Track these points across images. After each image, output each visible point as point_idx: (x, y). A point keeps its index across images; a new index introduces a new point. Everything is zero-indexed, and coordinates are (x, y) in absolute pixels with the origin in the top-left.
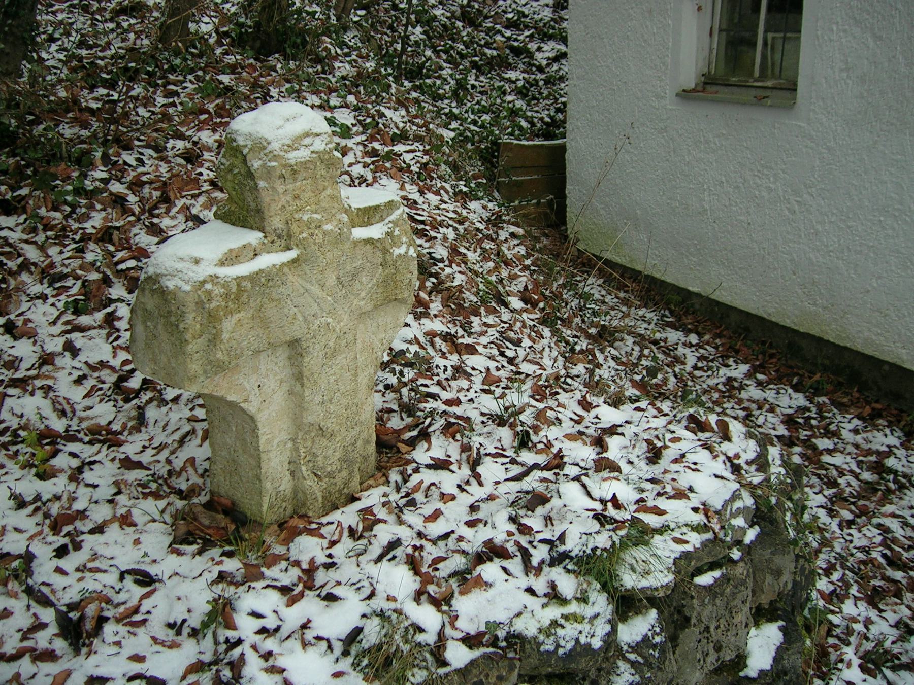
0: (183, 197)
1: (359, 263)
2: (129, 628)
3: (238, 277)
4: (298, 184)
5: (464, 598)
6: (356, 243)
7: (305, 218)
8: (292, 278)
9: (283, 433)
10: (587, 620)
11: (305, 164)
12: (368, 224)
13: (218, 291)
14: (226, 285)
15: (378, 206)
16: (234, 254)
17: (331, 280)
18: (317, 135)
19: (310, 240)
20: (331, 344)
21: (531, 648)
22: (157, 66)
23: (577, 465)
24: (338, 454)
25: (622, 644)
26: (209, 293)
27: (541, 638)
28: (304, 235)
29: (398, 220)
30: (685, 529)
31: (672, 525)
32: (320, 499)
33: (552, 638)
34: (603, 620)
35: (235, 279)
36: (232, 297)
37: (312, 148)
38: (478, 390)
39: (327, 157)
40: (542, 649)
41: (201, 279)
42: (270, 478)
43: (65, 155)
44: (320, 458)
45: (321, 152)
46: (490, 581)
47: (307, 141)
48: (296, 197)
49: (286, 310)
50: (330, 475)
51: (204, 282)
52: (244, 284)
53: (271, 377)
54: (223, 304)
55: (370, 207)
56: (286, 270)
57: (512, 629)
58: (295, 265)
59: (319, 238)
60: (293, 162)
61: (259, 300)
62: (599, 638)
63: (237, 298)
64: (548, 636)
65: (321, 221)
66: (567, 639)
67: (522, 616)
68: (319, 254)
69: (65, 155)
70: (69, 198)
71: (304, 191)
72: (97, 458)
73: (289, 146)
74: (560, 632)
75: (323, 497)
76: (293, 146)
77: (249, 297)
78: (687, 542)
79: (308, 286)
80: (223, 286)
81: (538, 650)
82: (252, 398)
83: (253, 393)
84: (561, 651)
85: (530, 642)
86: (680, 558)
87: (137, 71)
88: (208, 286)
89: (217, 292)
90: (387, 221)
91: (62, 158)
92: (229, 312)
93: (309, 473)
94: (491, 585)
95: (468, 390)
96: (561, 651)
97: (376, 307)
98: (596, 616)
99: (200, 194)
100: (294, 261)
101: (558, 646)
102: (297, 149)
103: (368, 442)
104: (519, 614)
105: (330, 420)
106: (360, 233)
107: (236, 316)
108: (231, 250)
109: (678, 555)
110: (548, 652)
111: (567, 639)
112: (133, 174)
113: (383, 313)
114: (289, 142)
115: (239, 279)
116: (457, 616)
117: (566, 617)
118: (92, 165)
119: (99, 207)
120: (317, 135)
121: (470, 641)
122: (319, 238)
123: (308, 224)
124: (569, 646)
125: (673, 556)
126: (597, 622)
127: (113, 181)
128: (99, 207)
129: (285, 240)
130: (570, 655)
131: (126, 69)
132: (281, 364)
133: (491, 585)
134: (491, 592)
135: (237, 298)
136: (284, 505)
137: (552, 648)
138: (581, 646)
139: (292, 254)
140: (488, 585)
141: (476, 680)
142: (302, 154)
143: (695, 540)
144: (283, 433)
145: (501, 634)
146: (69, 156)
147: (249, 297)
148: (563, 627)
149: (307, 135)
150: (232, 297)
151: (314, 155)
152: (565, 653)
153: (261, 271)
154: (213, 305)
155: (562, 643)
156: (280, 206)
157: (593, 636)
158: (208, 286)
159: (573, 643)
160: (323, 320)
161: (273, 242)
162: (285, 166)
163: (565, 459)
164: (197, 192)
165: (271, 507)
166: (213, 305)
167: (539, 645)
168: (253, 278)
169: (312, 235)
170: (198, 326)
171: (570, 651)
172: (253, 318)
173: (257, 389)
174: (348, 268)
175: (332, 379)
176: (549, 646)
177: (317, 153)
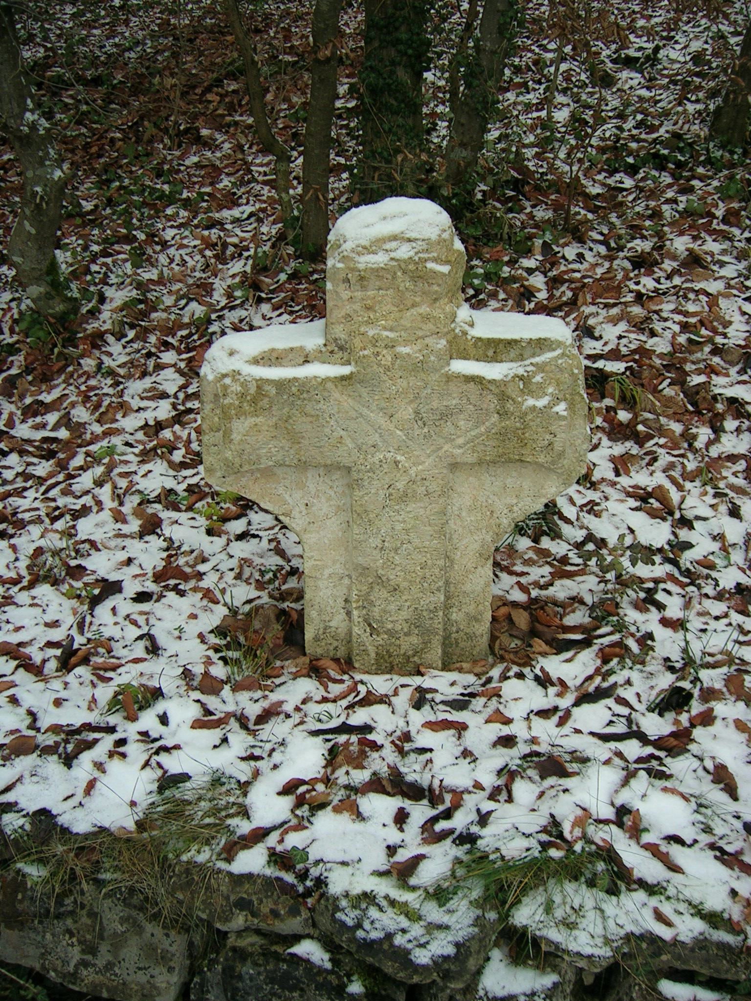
0: (593, 304)
1: (454, 402)
2: (95, 679)
3: (261, 379)
4: (370, 293)
5: (332, 814)
6: (450, 378)
7: (371, 333)
8: (341, 399)
9: (338, 565)
10: (422, 923)
11: (377, 272)
12: (495, 359)
13: (237, 388)
14: (244, 384)
15: (516, 341)
16: (275, 355)
17: (406, 412)
18: (409, 240)
19: (373, 359)
20: (400, 485)
21: (326, 907)
22: (692, 157)
23: (701, 760)
24: (405, 614)
25: (480, 986)
26: (225, 387)
27: (344, 903)
28: (366, 352)
29: (545, 364)
30: (682, 907)
31: (671, 891)
32: (373, 655)
33: (357, 912)
34: (450, 938)
35: (257, 381)
36: (249, 398)
37: (393, 255)
38: (734, 623)
39: (412, 267)
40: (339, 915)
41: (224, 372)
42: (316, 607)
43: (506, 237)
44: (376, 609)
45: (405, 261)
46: (365, 815)
47: (393, 245)
48: (368, 308)
49: (327, 431)
50: (391, 633)
51: (225, 376)
52: (267, 388)
53: (323, 500)
54: (237, 403)
55: (500, 341)
56: (329, 385)
57: (325, 874)
58: (344, 383)
59: (387, 358)
60: (361, 266)
61: (286, 409)
62: (429, 954)
63: (254, 401)
64: (354, 907)
65: (392, 340)
66: (377, 925)
67: (345, 868)
68: (385, 378)
69: (506, 237)
70: (476, 282)
71: (380, 302)
72: (260, 533)
73: (365, 248)
74: (373, 912)
75: (377, 654)
76: (370, 249)
77: (271, 403)
78: (669, 924)
79: (365, 411)
80: (242, 385)
81: (333, 915)
82: (295, 513)
83: (298, 509)
84: (360, 934)
85: (327, 899)
86: (641, 937)
87: (665, 158)
88: (228, 381)
89: (233, 389)
90: (527, 362)
91: (501, 239)
92: (241, 413)
93: (360, 620)
94: (364, 819)
95: (717, 618)
96: (360, 934)
97: (480, 463)
98: (445, 927)
99: (615, 305)
100: (343, 378)
101: (359, 926)
102: (374, 253)
103: (475, 619)
104: (344, 863)
105: (394, 572)
106: (461, 366)
107: (251, 421)
108: (273, 350)
109: (637, 931)
110: (343, 924)
111: (377, 925)
112: (563, 268)
113: (514, 474)
114: (367, 244)
115: (261, 383)
116: (307, 828)
117: (393, 903)
118: (528, 252)
119: (502, 296)
120: (409, 240)
121: (278, 859)
122: (387, 358)
123: (374, 341)
124: (375, 935)
125: (629, 928)
126: (440, 935)
127: (537, 273)
128: (502, 296)
129: (336, 349)
130: (369, 945)
131: (656, 155)
132: (340, 490)
133: (364, 819)
134: (359, 826)
135: (254, 401)
136: (335, 644)
137: (350, 923)
138: (392, 945)
139: (346, 370)
140: (360, 817)
141: (245, 896)
142: (380, 259)
143: (689, 928)
144: (338, 565)
145: (314, 872)
146: (510, 238)
147: (271, 403)
148: (381, 909)
149: (394, 238)
150: (249, 398)
151: (395, 263)
152: (364, 939)
153: (296, 379)
154: (227, 401)
155: (367, 925)
156: (343, 313)
157: (423, 946)
158: (228, 381)
159: (381, 935)
160: (389, 455)
161: (332, 352)
162: (353, 270)
163: (692, 747)
164: (612, 301)
165: (317, 639)
166: (227, 401)
167: (337, 909)
168: (281, 385)
169: (378, 354)
170: (216, 419)
171: (373, 941)
172: (276, 426)
173: (303, 508)
174: (435, 404)
175: (399, 527)
176: (348, 917)
177: (397, 260)
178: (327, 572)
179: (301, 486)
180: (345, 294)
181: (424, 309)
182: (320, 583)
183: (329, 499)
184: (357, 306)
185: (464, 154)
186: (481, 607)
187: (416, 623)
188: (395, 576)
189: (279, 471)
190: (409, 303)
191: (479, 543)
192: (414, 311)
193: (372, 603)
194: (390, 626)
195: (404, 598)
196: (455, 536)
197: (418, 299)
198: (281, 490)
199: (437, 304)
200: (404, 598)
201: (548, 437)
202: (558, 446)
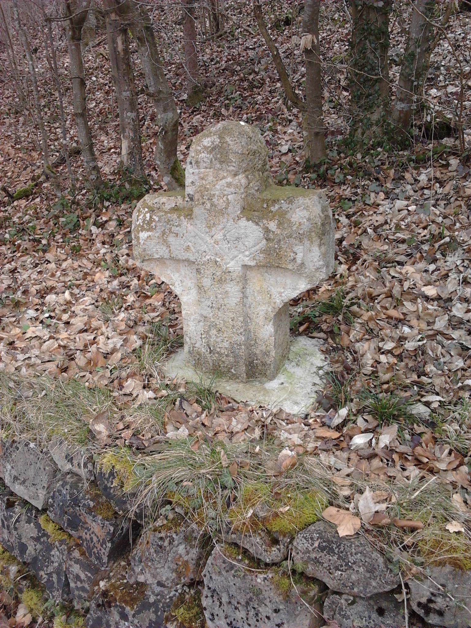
32: (211, 364)
48: (203, 179)
71: (207, 175)
79: (199, 233)
82: (176, 284)
113: (281, 275)
178: (192, 318)
179: (178, 271)
180: (191, 171)
181: (229, 179)
182: (189, 323)
183: (191, 279)
184: (196, 177)
185: (403, 105)
186: (268, 348)
187: (232, 351)
188: (220, 323)
189: (167, 262)
190: (221, 176)
191: (265, 311)
192: (224, 181)
193: (210, 336)
194: (218, 350)
195: (224, 336)
196: (252, 306)
197: (225, 174)
198: (169, 272)
199: (237, 177)
200: (224, 336)
201: (292, 254)
202: (299, 261)
